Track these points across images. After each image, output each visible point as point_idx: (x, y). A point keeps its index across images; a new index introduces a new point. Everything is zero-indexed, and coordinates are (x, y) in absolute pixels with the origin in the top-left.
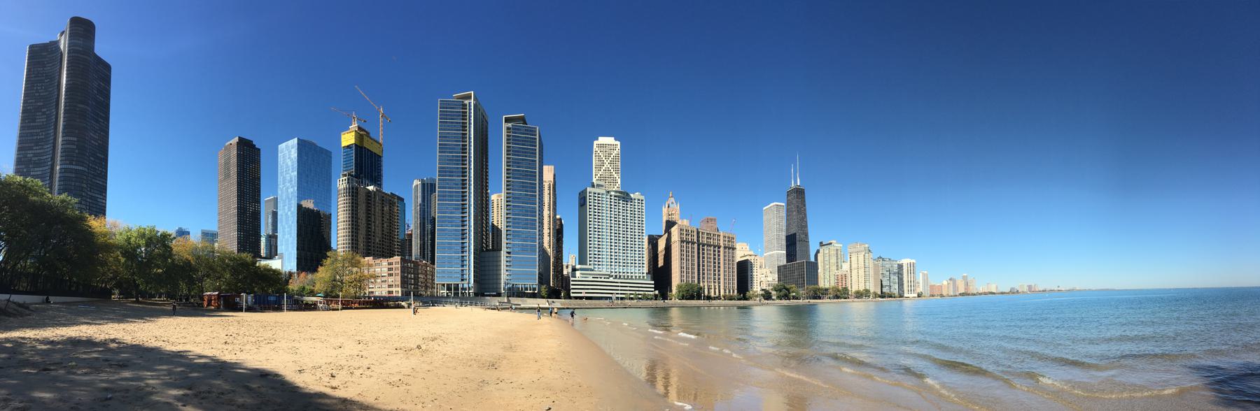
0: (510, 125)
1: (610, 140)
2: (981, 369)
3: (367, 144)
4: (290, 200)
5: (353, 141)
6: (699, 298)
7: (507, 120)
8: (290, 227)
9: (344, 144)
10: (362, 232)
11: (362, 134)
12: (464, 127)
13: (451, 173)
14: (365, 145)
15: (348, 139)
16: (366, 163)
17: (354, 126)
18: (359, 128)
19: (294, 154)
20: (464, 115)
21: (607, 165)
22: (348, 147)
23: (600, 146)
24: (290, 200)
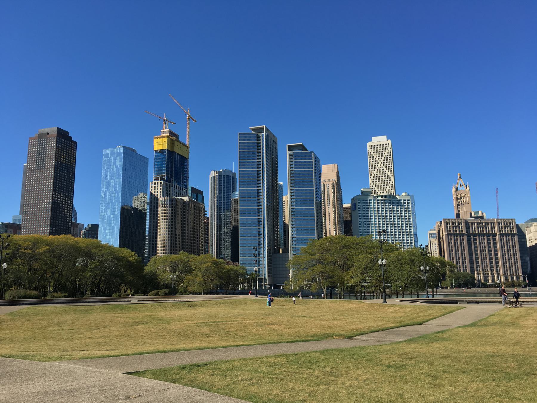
0: (292, 152)
1: (381, 140)
2: (228, 359)
3: (178, 150)
4: (113, 204)
5: (165, 147)
6: (474, 286)
7: (290, 148)
8: (113, 229)
9: (156, 148)
10: (179, 231)
11: (173, 138)
12: (258, 155)
13: (249, 194)
14: (176, 150)
15: (160, 144)
16: (175, 165)
17: (165, 131)
18: (171, 133)
19: (120, 162)
20: (258, 146)
21: (380, 164)
22: (161, 151)
23: (372, 147)
24: (113, 204)
